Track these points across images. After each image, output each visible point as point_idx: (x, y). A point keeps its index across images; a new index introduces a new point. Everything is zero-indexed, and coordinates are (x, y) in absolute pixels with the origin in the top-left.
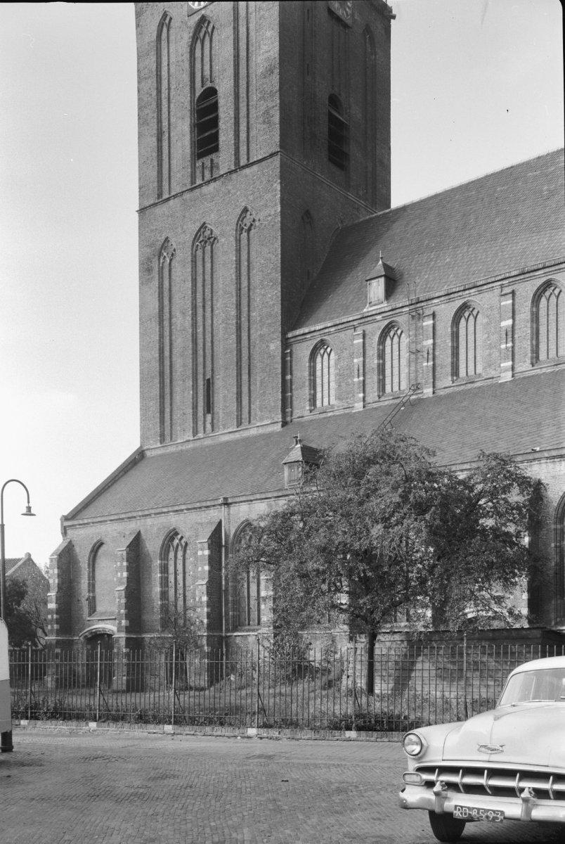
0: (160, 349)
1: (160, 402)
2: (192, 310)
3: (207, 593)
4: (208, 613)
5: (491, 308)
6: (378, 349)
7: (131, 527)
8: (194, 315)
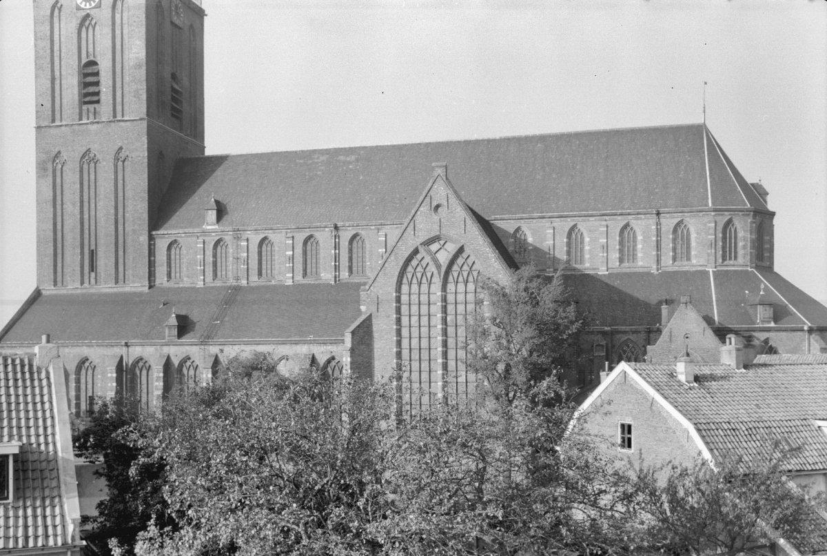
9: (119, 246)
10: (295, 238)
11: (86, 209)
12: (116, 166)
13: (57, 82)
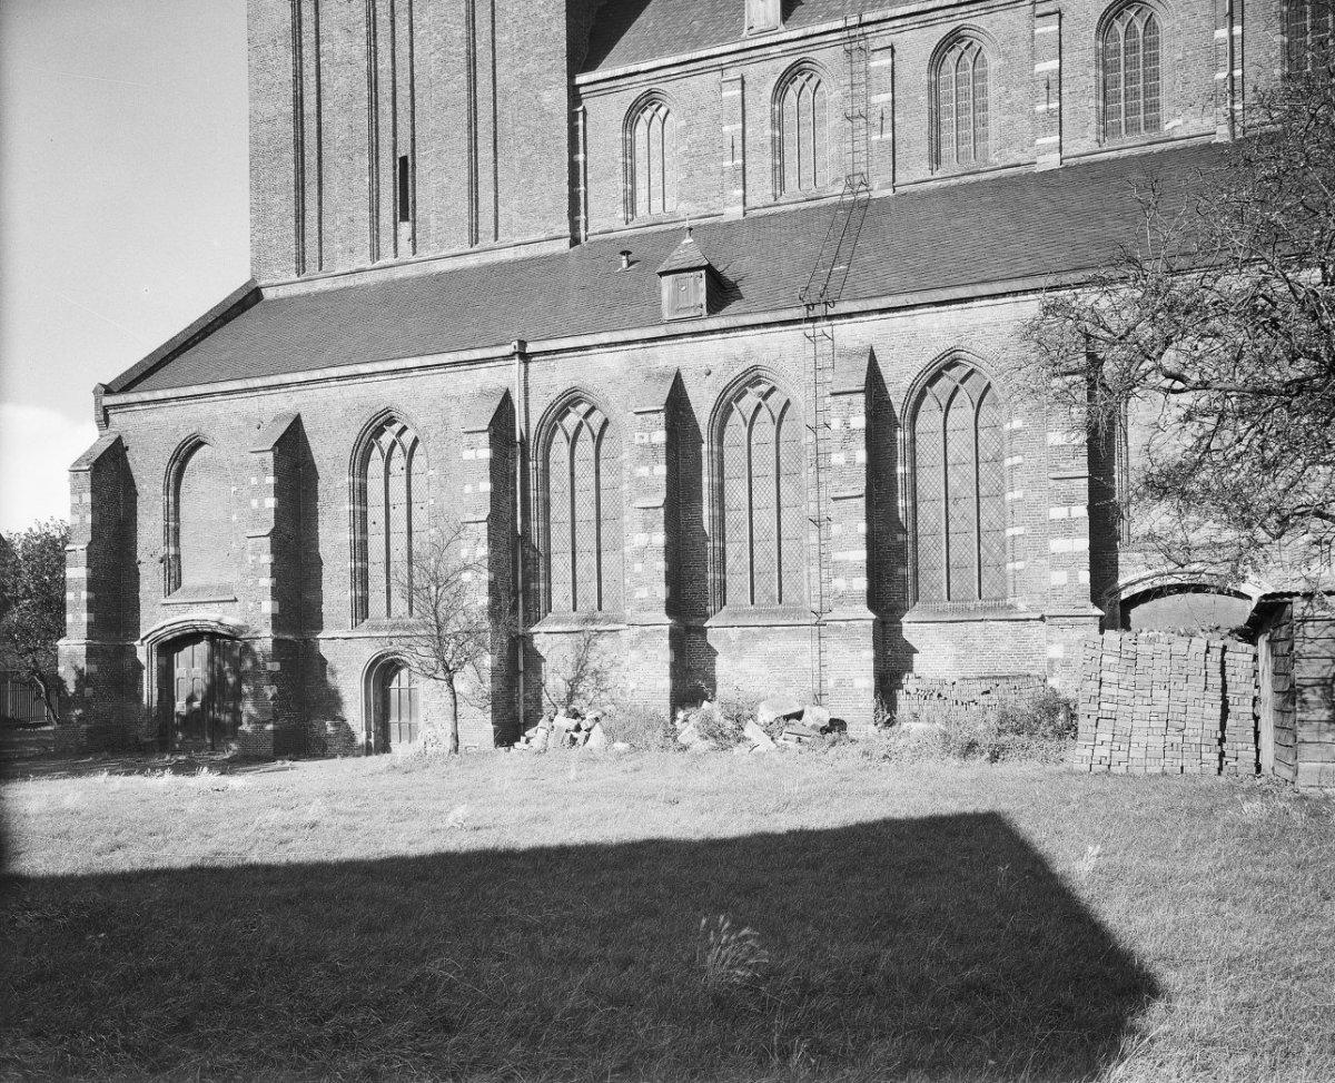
0: (295, 97)
1: (296, 197)
2: (368, 25)
3: (489, 539)
4: (88, 600)
5: (1013, 39)
6: (772, 109)
7: (275, 407)
8: (372, 36)
10: (1066, 15)
11: (385, 121)
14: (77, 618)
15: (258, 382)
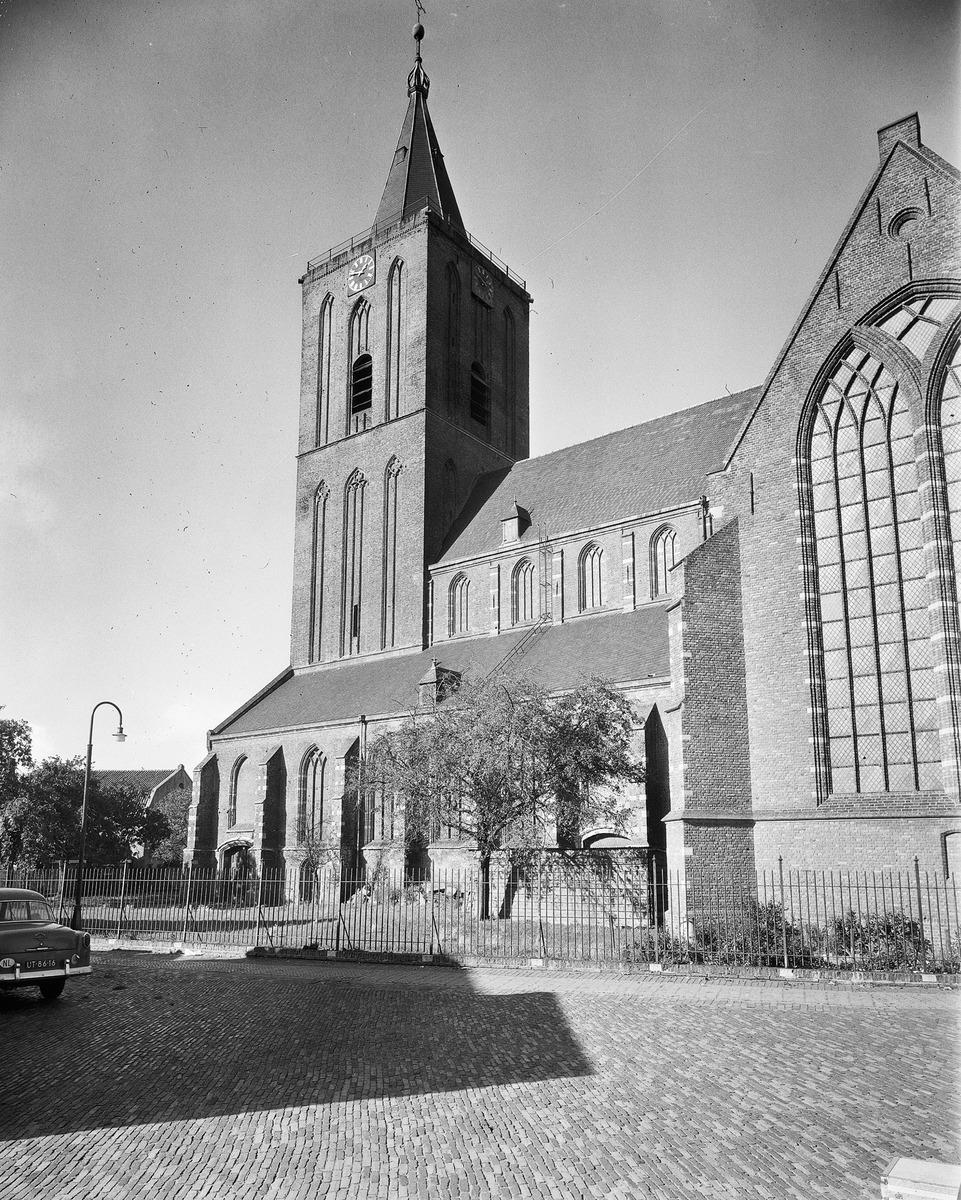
7: (272, 742)
9: (387, 595)
12: (386, 485)
13: (324, 395)
14: (191, 839)
15: (267, 731)
